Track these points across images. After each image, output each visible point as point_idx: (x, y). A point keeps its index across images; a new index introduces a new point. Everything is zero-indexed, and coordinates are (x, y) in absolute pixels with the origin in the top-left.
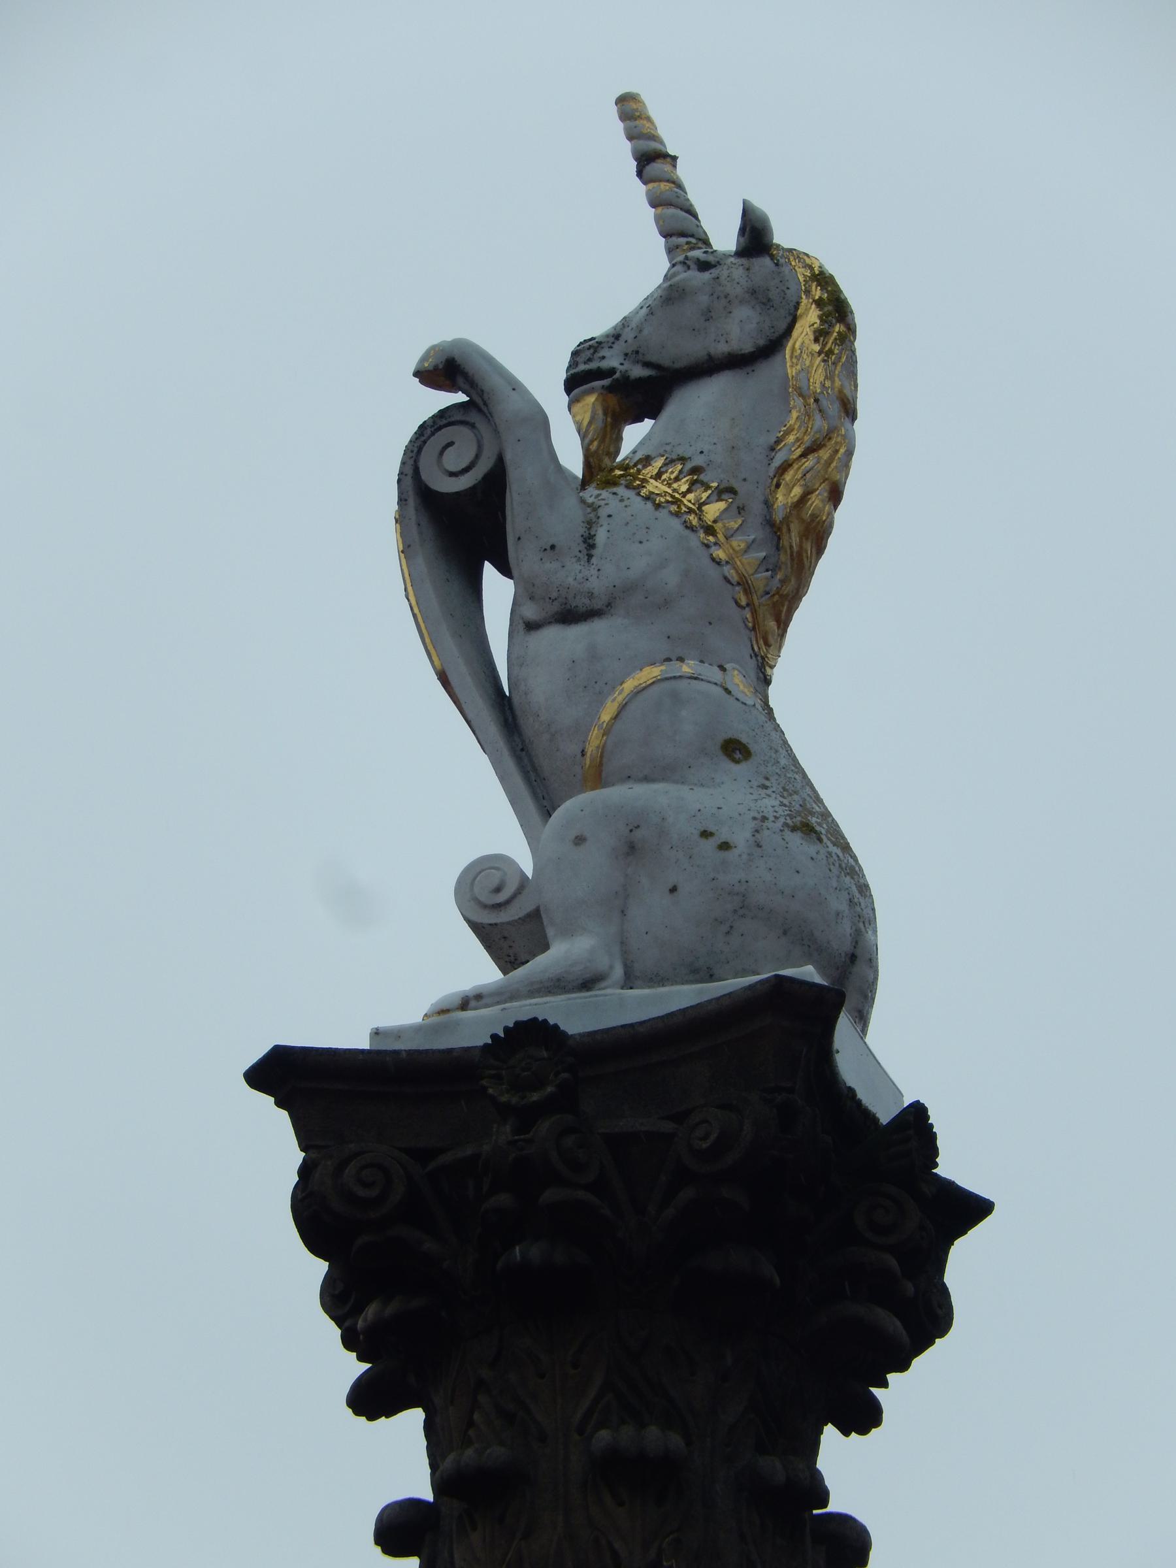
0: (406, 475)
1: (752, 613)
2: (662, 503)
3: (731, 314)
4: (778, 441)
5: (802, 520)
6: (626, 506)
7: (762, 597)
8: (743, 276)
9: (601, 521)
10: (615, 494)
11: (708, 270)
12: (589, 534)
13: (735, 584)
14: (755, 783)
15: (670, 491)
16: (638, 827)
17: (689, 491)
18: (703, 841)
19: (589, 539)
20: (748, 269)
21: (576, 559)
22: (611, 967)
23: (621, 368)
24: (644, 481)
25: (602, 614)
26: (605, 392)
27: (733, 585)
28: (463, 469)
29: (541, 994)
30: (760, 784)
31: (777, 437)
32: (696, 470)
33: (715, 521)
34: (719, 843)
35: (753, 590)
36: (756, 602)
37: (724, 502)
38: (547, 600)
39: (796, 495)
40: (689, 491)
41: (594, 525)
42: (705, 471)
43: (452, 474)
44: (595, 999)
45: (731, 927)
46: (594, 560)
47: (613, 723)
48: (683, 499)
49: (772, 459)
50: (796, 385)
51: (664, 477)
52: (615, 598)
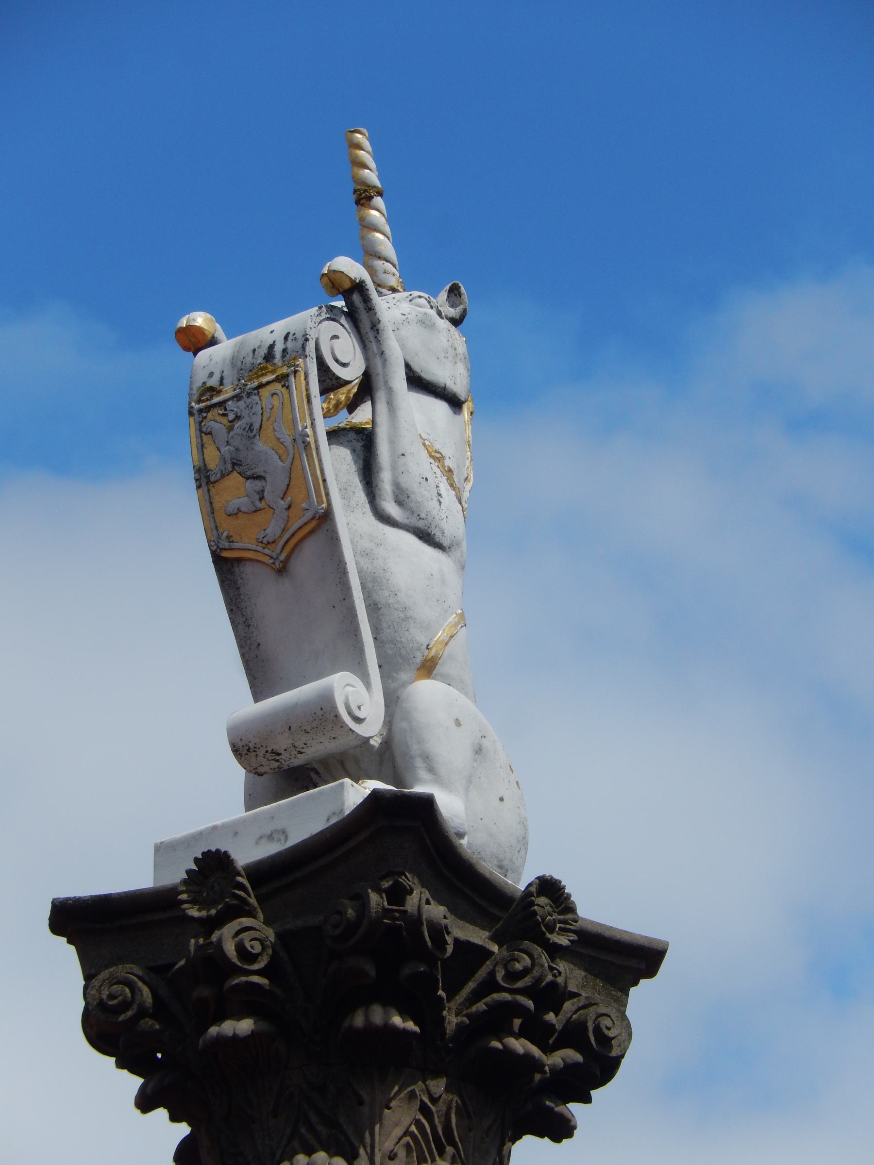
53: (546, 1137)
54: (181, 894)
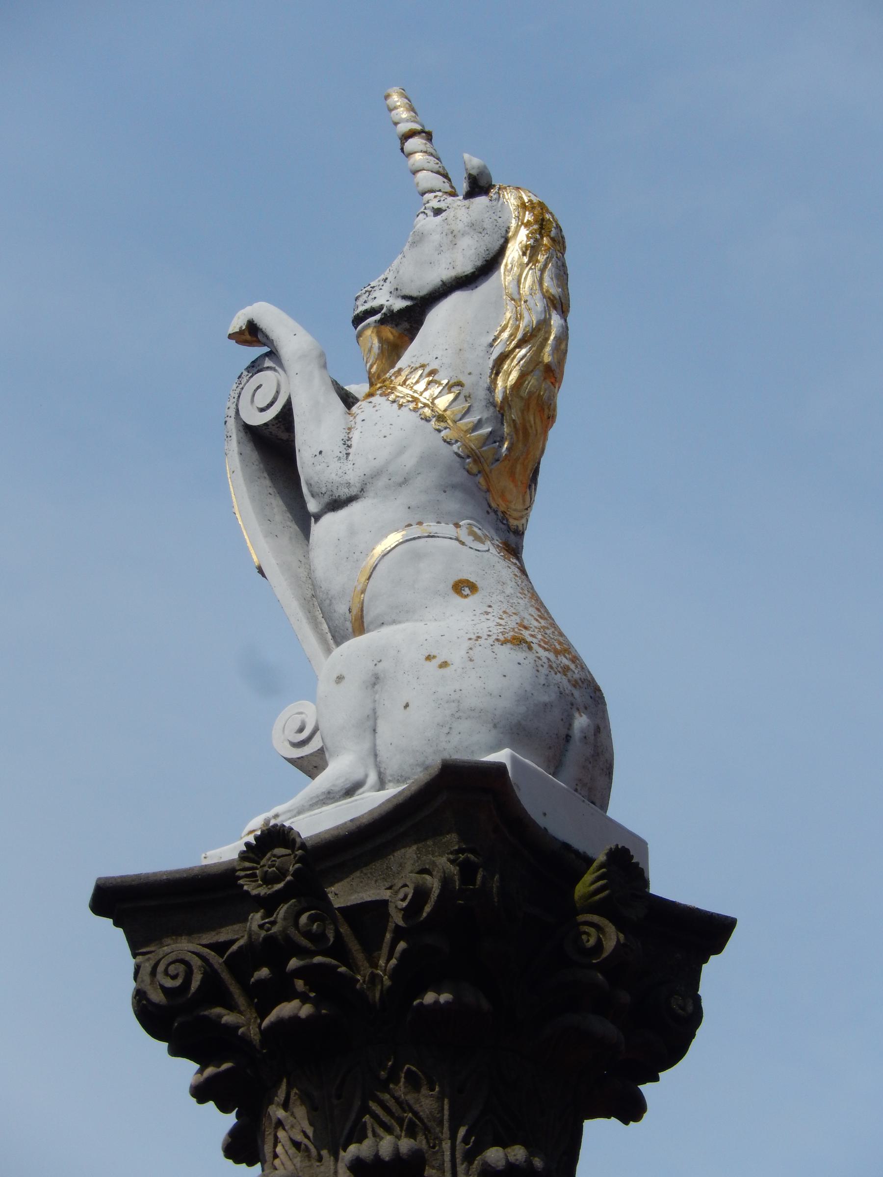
0: (230, 417)
1: (485, 479)
2: (404, 403)
3: (456, 246)
4: (495, 340)
5: (522, 398)
6: (377, 411)
7: (492, 464)
8: (465, 214)
9: (358, 426)
10: (370, 402)
11: (440, 215)
12: (348, 437)
13: (465, 457)
14: (478, 612)
15: (411, 393)
16: (380, 661)
17: (426, 389)
18: (428, 663)
19: (348, 441)
20: (468, 208)
21: (338, 458)
22: (366, 776)
23: (387, 304)
24: (394, 388)
25: (358, 499)
26: (377, 324)
27: (463, 458)
28: (268, 405)
29: (318, 806)
30: (483, 612)
31: (495, 336)
32: (433, 372)
33: (445, 410)
34: (440, 663)
35: (482, 460)
36: (487, 469)
37: (453, 394)
38: (320, 495)
39: (513, 379)
40: (426, 389)
41: (352, 430)
42: (438, 372)
43: (262, 410)
44: (355, 803)
45: (450, 728)
46: (350, 457)
47: (368, 583)
48: (420, 397)
49: (491, 354)
50: (508, 293)
51: (407, 383)
52: (366, 484)
53: (236, 1120)
54: (262, 1024)
